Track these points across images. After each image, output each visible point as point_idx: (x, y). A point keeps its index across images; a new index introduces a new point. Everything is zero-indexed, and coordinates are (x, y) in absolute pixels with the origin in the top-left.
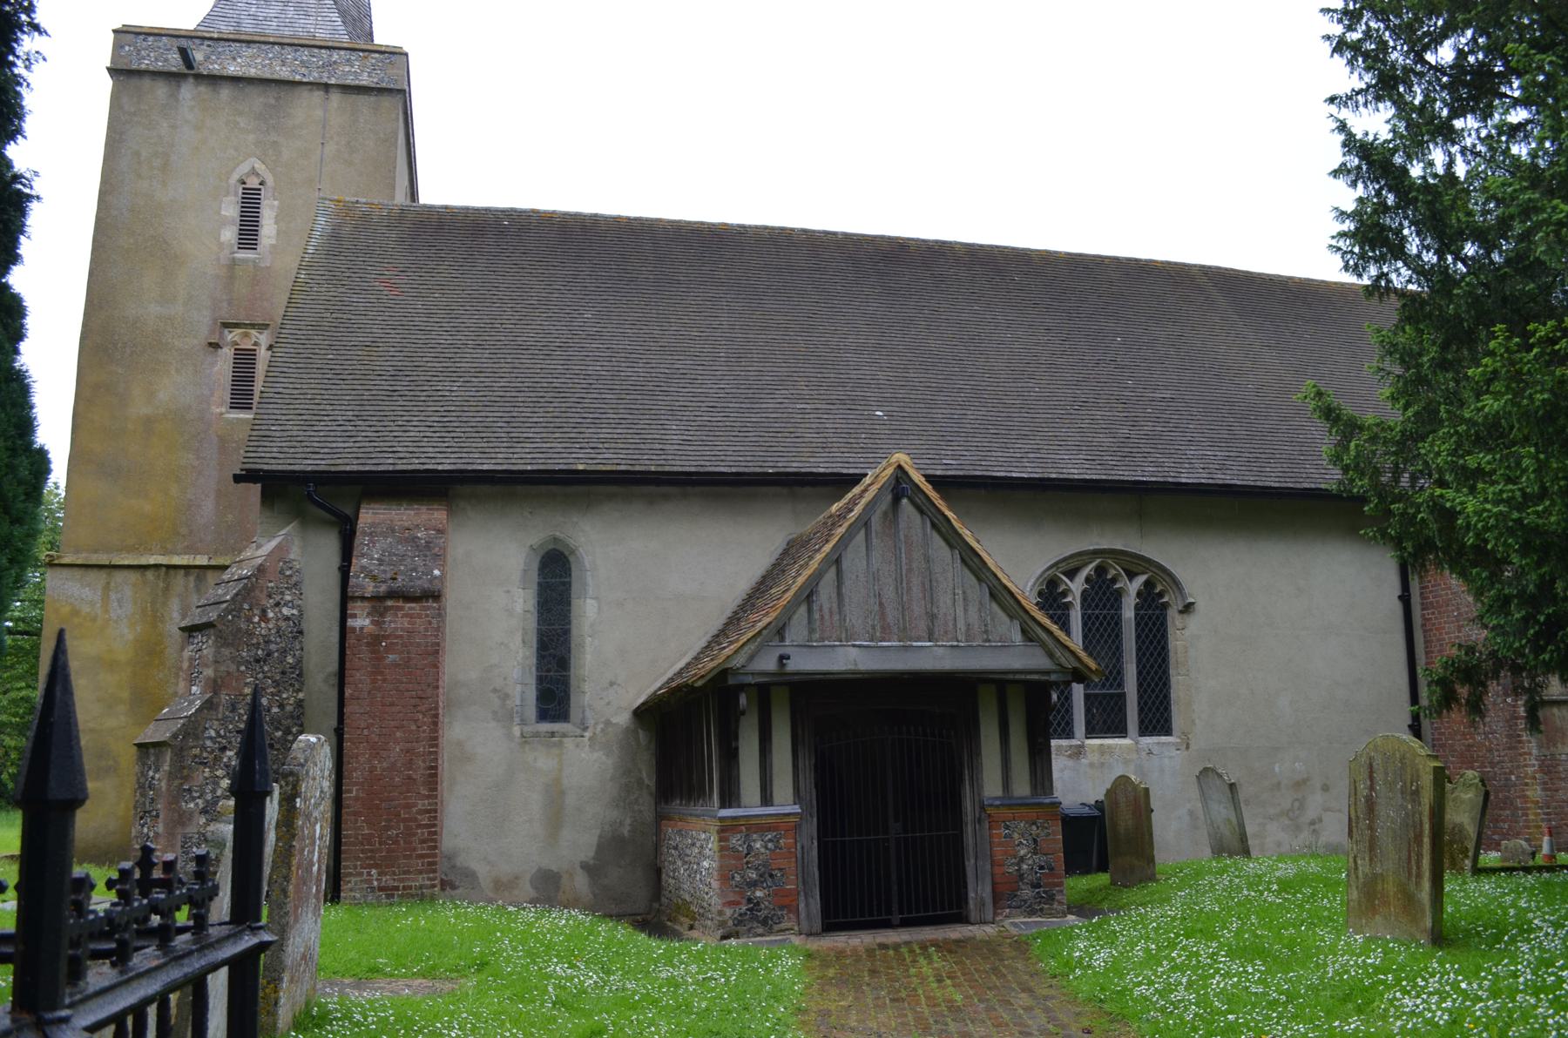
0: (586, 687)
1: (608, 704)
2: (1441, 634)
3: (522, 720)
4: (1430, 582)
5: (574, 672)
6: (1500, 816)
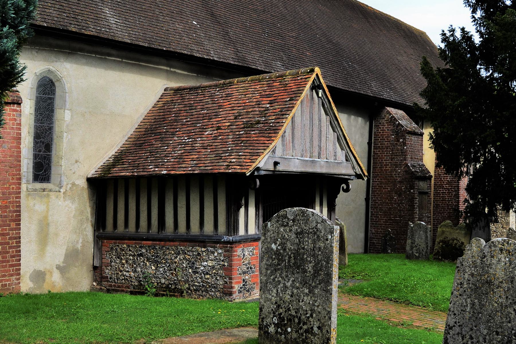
0: (63, 162)
1: (74, 173)
2: (382, 160)
3: (27, 181)
4: (380, 137)
5: (54, 153)
6: (401, 237)
